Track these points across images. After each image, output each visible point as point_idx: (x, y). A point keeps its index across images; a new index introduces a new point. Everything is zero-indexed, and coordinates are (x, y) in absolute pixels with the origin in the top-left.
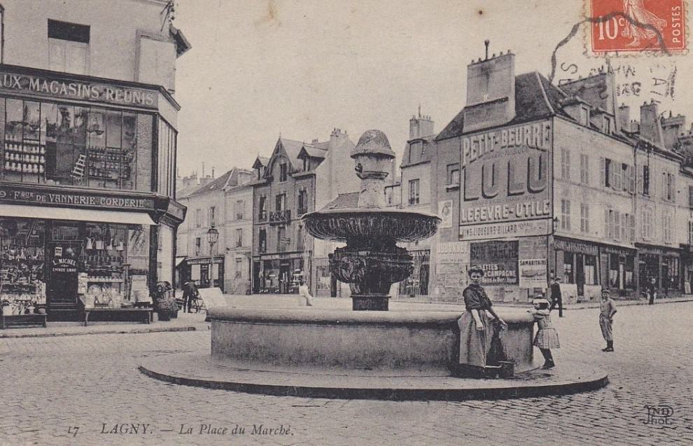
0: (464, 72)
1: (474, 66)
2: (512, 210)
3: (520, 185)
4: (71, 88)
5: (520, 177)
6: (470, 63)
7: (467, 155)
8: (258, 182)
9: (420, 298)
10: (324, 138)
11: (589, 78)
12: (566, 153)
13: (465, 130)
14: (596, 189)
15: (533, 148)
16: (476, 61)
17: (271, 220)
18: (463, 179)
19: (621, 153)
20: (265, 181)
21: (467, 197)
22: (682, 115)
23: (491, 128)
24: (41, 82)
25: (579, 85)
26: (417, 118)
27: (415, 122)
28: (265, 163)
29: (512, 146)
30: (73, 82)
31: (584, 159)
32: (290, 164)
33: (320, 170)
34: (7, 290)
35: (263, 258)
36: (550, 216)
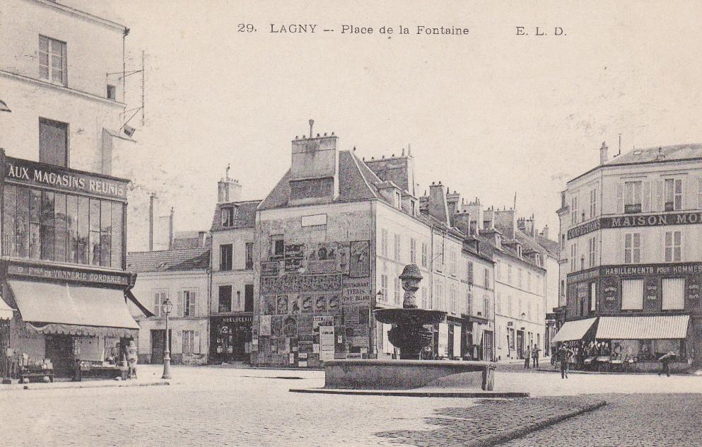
0: (289, 148)
4: (64, 179)
9: (128, 380)
12: (384, 232)
16: (300, 138)
22: (458, 192)
24: (43, 174)
27: (223, 186)
30: (67, 174)
31: (397, 238)
34: (124, 355)
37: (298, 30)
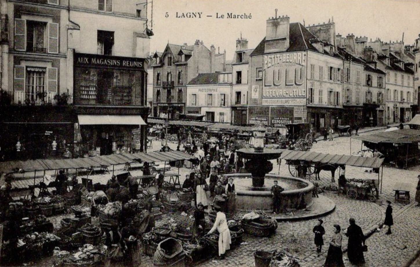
1: (270, 21)
2: (288, 93)
3: (292, 81)
5: (292, 77)
6: (268, 19)
7: (266, 64)
8: (156, 65)
10: (191, 43)
11: (324, 25)
12: (312, 66)
13: (266, 51)
14: (326, 82)
15: (297, 64)
17: (164, 86)
18: (264, 76)
19: (337, 63)
20: (160, 65)
21: (266, 85)
22: (366, 37)
23: (277, 52)
24: (96, 60)
25: (318, 28)
26: (240, 39)
27: (239, 42)
28: (160, 55)
29: (288, 62)
31: (402, 92)
32: (174, 58)
33: (190, 61)
35: (159, 105)
36: (305, 97)
37: (191, 16)
